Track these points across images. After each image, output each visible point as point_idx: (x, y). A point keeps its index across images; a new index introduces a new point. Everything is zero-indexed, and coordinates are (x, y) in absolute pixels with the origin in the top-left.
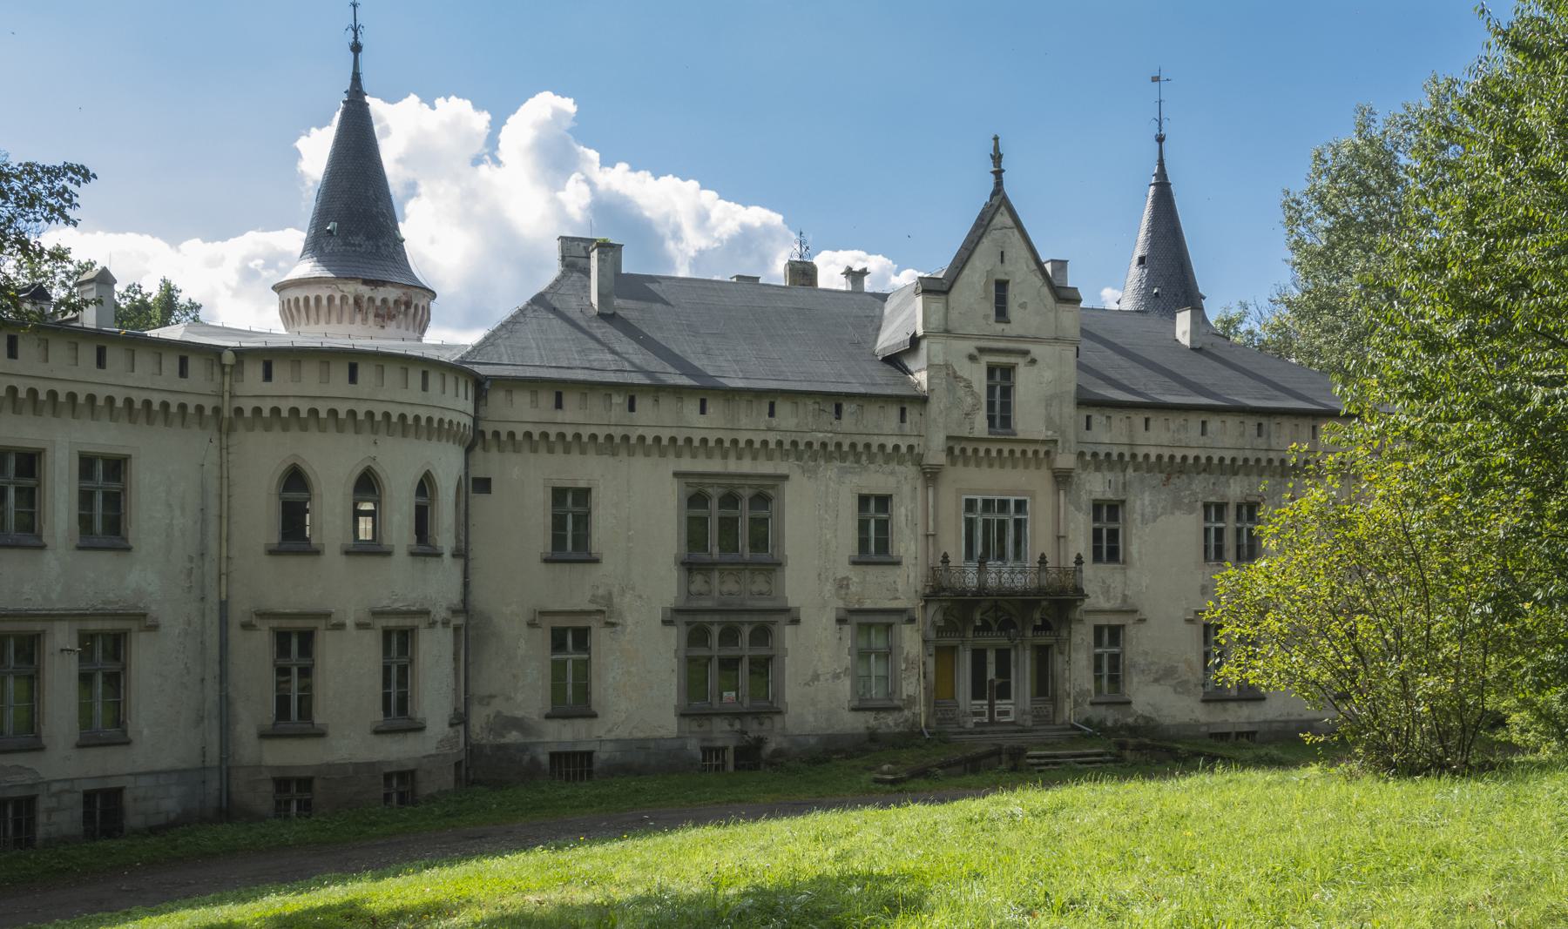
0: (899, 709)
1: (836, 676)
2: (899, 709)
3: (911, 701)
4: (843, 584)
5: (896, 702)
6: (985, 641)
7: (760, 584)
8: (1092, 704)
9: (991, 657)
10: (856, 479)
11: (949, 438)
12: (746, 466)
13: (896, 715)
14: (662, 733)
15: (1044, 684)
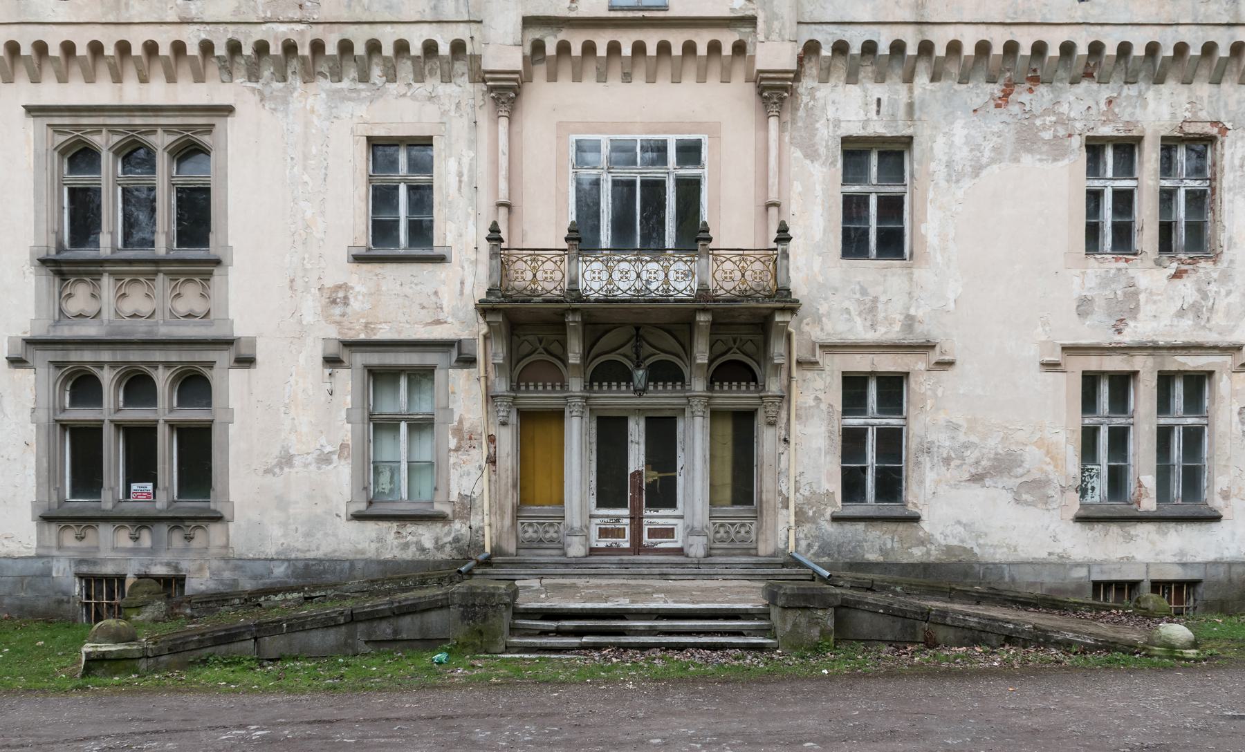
0: (440, 518)
1: (324, 459)
2: (440, 518)
3: (467, 506)
4: (337, 297)
5: (438, 507)
6: (615, 398)
7: (190, 299)
8: (836, 519)
9: (636, 431)
10: (362, 110)
11: (529, 22)
12: (157, 92)
14: (14, 548)
15: (741, 482)
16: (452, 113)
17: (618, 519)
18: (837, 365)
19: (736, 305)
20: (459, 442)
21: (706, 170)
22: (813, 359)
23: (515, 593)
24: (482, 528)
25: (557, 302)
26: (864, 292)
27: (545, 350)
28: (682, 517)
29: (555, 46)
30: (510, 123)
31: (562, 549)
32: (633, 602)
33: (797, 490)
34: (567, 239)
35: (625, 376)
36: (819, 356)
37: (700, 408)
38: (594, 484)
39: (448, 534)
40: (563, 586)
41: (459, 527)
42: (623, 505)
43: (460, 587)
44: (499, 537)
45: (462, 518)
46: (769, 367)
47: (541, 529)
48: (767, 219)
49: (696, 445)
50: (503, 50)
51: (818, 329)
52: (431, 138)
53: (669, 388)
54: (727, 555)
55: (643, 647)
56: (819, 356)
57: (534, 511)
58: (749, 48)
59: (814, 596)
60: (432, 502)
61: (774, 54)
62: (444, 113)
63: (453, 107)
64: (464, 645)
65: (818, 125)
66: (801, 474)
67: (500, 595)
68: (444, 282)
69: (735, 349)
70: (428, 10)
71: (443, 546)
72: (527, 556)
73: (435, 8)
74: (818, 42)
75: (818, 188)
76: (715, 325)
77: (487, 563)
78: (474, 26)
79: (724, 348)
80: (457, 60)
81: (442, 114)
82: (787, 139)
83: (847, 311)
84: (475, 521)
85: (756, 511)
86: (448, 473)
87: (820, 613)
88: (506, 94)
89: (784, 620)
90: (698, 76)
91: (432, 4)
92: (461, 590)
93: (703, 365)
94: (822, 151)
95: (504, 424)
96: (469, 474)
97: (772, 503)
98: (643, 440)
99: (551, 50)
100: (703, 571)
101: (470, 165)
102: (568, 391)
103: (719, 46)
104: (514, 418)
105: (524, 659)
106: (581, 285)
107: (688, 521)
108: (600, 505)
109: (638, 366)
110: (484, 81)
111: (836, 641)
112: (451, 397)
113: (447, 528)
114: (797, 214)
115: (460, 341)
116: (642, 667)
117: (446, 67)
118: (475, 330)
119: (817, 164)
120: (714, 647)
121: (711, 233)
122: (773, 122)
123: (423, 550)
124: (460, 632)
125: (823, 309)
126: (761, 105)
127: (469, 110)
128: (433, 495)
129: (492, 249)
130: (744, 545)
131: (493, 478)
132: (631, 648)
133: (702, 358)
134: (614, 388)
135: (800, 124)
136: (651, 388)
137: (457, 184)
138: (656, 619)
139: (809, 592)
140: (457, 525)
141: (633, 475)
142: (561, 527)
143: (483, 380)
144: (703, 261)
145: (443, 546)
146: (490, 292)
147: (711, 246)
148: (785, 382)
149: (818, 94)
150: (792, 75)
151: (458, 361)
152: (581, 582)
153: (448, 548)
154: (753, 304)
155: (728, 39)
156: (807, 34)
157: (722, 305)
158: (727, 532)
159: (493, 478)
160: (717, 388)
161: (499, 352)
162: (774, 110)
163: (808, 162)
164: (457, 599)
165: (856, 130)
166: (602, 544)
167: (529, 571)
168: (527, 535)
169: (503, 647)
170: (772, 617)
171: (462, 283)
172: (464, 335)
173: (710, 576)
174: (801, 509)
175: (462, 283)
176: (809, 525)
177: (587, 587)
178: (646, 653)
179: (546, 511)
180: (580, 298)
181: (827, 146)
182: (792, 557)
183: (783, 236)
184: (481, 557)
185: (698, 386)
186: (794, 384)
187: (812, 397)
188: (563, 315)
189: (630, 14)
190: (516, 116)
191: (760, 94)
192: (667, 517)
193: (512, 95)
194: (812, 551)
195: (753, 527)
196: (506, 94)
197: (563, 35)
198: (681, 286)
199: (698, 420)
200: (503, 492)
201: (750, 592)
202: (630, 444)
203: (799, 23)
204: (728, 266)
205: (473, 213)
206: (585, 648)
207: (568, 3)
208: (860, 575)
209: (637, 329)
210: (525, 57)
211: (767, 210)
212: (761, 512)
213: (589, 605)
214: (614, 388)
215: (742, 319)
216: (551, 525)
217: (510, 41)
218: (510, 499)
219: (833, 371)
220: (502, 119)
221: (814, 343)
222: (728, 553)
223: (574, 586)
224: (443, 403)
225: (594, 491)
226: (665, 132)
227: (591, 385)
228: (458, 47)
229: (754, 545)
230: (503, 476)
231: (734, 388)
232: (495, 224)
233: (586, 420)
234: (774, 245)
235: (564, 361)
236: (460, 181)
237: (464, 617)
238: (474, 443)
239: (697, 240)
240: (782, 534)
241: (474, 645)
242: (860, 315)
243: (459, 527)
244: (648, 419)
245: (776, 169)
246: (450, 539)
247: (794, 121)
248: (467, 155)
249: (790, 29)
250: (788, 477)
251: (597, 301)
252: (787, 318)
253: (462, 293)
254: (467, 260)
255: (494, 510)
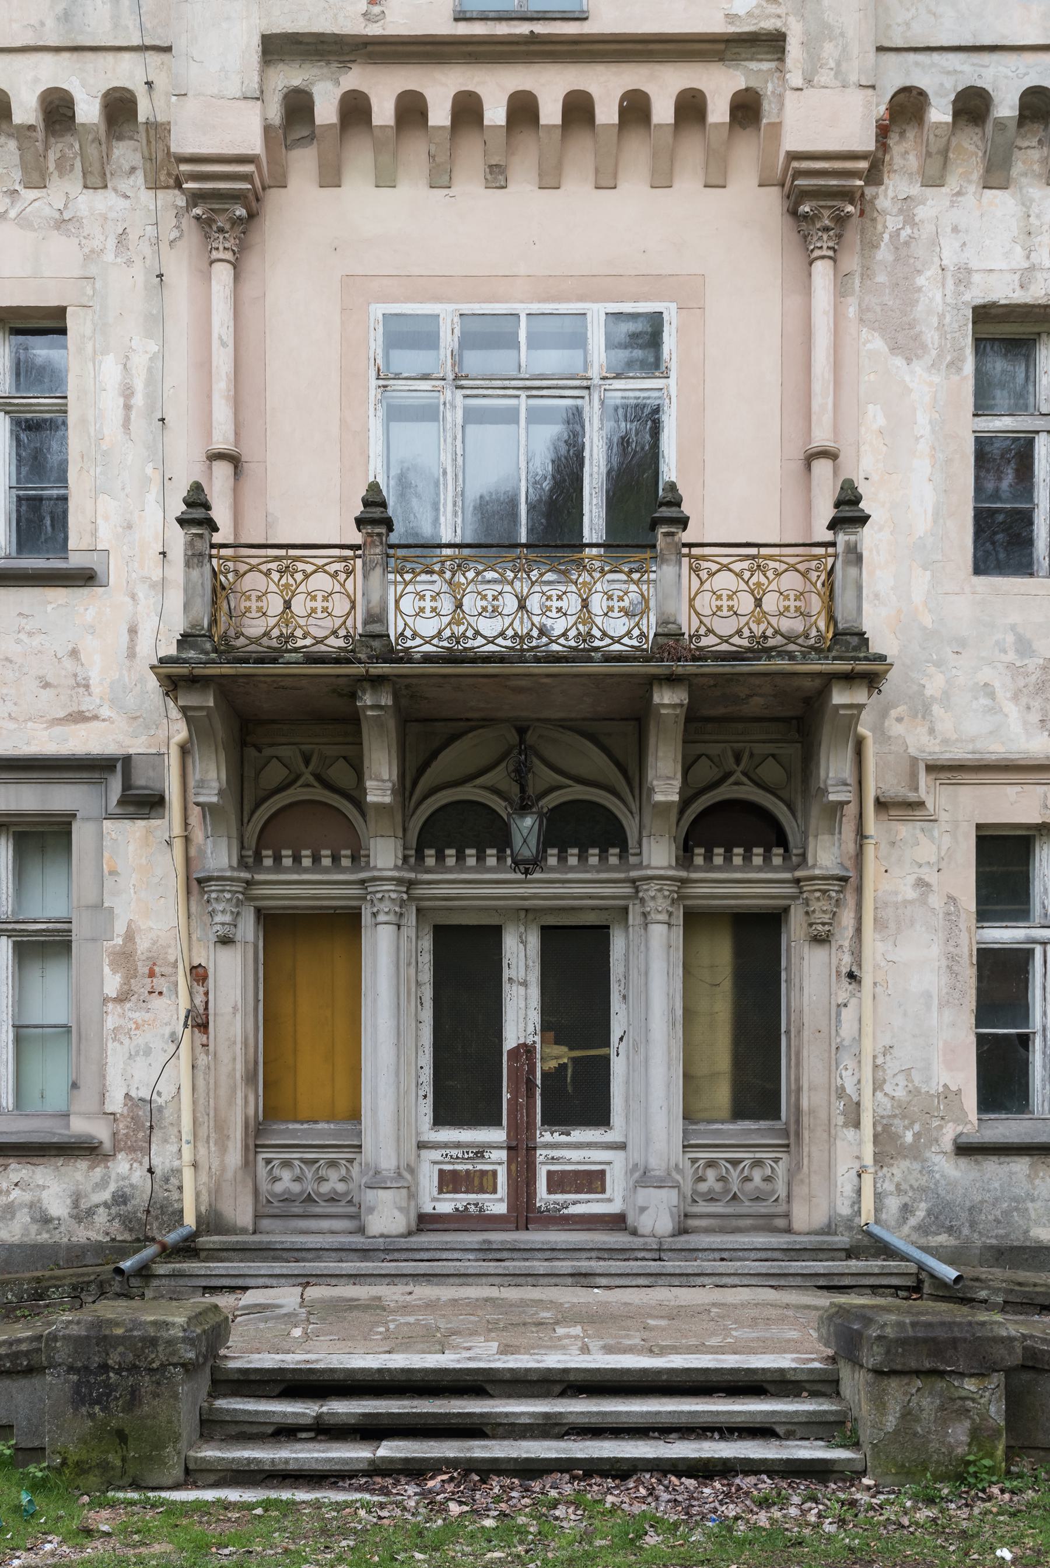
0: (84, 1149)
2: (84, 1149)
3: (144, 1122)
5: (80, 1126)
6: (472, 883)
8: (965, 1150)
9: (521, 957)
11: (277, 48)
13: (79, 1173)
15: (753, 1069)
16: (109, 257)
17: (480, 1151)
18: (963, 812)
19: (743, 667)
20: (127, 981)
21: (672, 382)
22: (912, 797)
23: (215, 1333)
24: (178, 1172)
25: (337, 661)
26: (1024, 647)
27: (318, 777)
28: (622, 1146)
29: (334, 102)
30: (236, 278)
31: (356, 1217)
32: (506, 1349)
33: (878, 1086)
34: (360, 522)
35: (492, 834)
36: (925, 788)
37: (662, 904)
38: (427, 1075)
39: (104, 1183)
40: (352, 1305)
41: (125, 1170)
42: (494, 1121)
43: (65, 1321)
44: (216, 1191)
45: (132, 1149)
46: (815, 811)
47: (309, 1174)
48: (808, 489)
49: (652, 985)
50: (220, 112)
51: (922, 730)
52: (60, 312)
53: (593, 860)
54: (723, 1231)
55: (529, 1471)
56: (925, 788)
57: (294, 1133)
58: (769, 108)
59: (954, 1342)
60: (67, 1116)
61: (824, 115)
62: (91, 256)
63: (111, 243)
64: (81, 1469)
65: (921, 281)
66: (888, 1050)
67: (170, 1342)
68: (91, 630)
69: (738, 776)
70: (50, 23)
71: (90, 1212)
72: (278, 1234)
73: (66, 17)
74: (922, 93)
75: (923, 419)
76: (696, 722)
77: (188, 1249)
78: (153, 58)
79: (714, 774)
80: (120, 138)
81: (87, 258)
82: (852, 311)
83: (988, 690)
84: (162, 1157)
85: (786, 1133)
86: (103, 1050)
87: (970, 1385)
88: (227, 208)
89: (879, 1404)
90: (654, 172)
91: (59, 8)
92: (75, 1330)
93: (668, 805)
94: (931, 337)
95: (225, 941)
96: (148, 1052)
97: (823, 1115)
98: (534, 977)
99: (326, 112)
100: (671, 1265)
101: (150, 370)
102: (367, 867)
103: (702, 102)
104: (248, 929)
105: (227, 1506)
106: (394, 627)
107: (635, 1153)
108: (440, 1120)
109: (524, 808)
110: (178, 185)
111: (1011, 1453)
112: (109, 883)
113: (99, 1171)
114: (875, 477)
115: (127, 760)
116: (522, 1531)
117: (93, 151)
118: (162, 734)
119: (918, 367)
120: (704, 1471)
121: (686, 508)
122: (822, 270)
123: (45, 1220)
124: (68, 1435)
125: (934, 685)
126: (795, 238)
127: (146, 249)
128: (69, 1102)
129: (190, 545)
130: (762, 1208)
131: (202, 1060)
132: (499, 1473)
133: (665, 783)
134: (471, 862)
135: (881, 278)
136: (552, 861)
137: (120, 412)
138: (562, 1394)
139: (941, 1334)
140: (122, 1165)
141: (514, 1053)
142: (355, 1170)
143: (178, 845)
144: (668, 571)
145: (90, 1212)
146: (186, 640)
147: (686, 537)
148: (851, 847)
149: (922, 213)
150: (863, 165)
151: (122, 802)
152: (391, 1293)
153: (101, 1217)
154: (781, 664)
155: (720, 85)
156: (898, 73)
157: (711, 667)
158: (722, 1179)
159: (202, 1060)
160: (699, 860)
161: (211, 777)
162: (826, 241)
163: (899, 361)
164: (62, 1353)
165: (1004, 291)
166: (446, 1207)
167: (278, 1268)
168: (279, 1187)
169: (178, 1473)
170: (846, 1389)
171: (133, 631)
172: (136, 745)
173: (686, 1279)
174: (886, 1128)
175: (133, 631)
176: (905, 1164)
177: (405, 1309)
178: (536, 1485)
179: (320, 1134)
180: (390, 655)
181: (941, 326)
182: (869, 1234)
183: (849, 513)
184: (172, 1237)
185: (658, 854)
186: (870, 851)
187: (911, 879)
188: (353, 696)
189: (502, 29)
190: (252, 262)
191: (793, 213)
192: (589, 1145)
193: (241, 212)
194: (913, 1221)
195: (781, 1169)
196: (227, 208)
197: (355, 78)
198: (618, 626)
199: (658, 932)
200: (223, 1092)
201: (783, 1319)
202: (506, 986)
203: (880, 49)
204: (725, 581)
205: (157, 477)
206: (384, 1473)
207: (363, 6)
208: (1023, 1275)
209: (522, 731)
210: (267, 129)
211: (808, 467)
212: (798, 1135)
213: (399, 1361)
214: (471, 862)
215: (756, 705)
216: (333, 1164)
217: (234, 88)
218: (240, 1108)
219: (956, 823)
220: (218, 267)
221: (914, 761)
222: (726, 1225)
223: (376, 1306)
224: (91, 898)
225: (428, 1089)
226: (581, 299)
227: (420, 857)
228: (119, 108)
229: (781, 1209)
230: (225, 1056)
231: (738, 861)
232: (197, 488)
233: (409, 930)
234: (828, 536)
235: (358, 802)
236: (128, 407)
237: (80, 1398)
238: (161, 984)
239: (655, 524)
240: (845, 1183)
241: (104, 1467)
242: (1016, 697)
243: (125, 1170)
244: (547, 932)
245: (829, 376)
246: (106, 1195)
247: (867, 273)
248: (143, 350)
249: (860, 61)
250: (858, 1056)
251: (427, 658)
252: (859, 696)
253: (132, 654)
254: (144, 579)
255: (203, 1132)
